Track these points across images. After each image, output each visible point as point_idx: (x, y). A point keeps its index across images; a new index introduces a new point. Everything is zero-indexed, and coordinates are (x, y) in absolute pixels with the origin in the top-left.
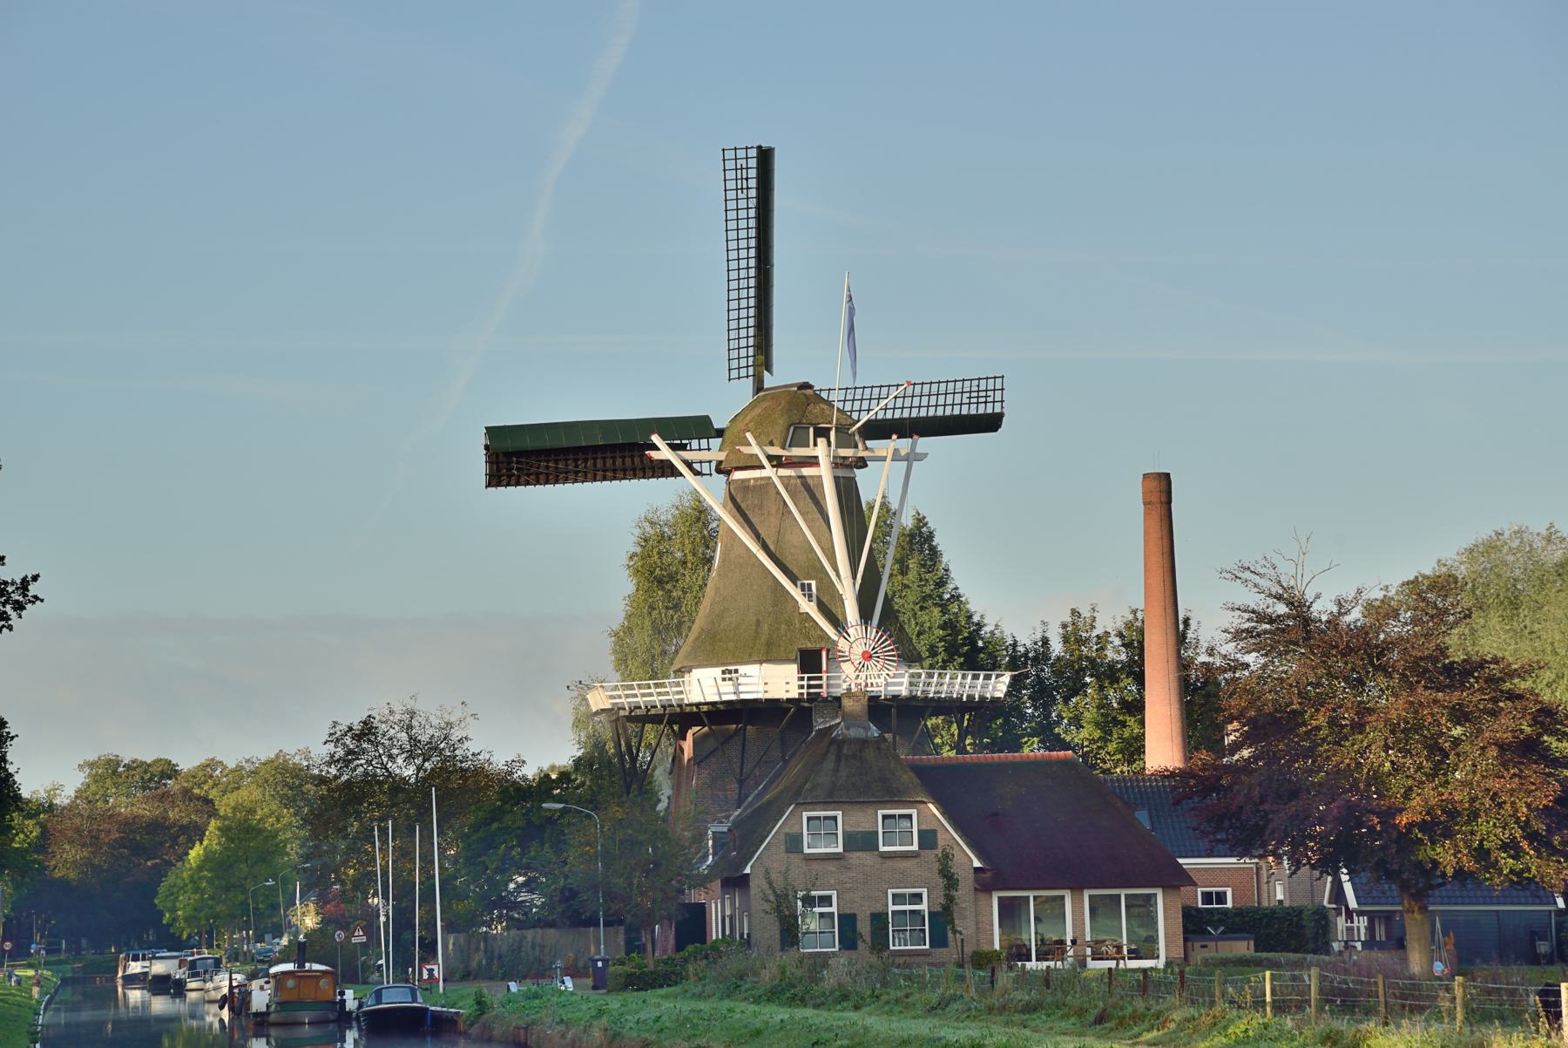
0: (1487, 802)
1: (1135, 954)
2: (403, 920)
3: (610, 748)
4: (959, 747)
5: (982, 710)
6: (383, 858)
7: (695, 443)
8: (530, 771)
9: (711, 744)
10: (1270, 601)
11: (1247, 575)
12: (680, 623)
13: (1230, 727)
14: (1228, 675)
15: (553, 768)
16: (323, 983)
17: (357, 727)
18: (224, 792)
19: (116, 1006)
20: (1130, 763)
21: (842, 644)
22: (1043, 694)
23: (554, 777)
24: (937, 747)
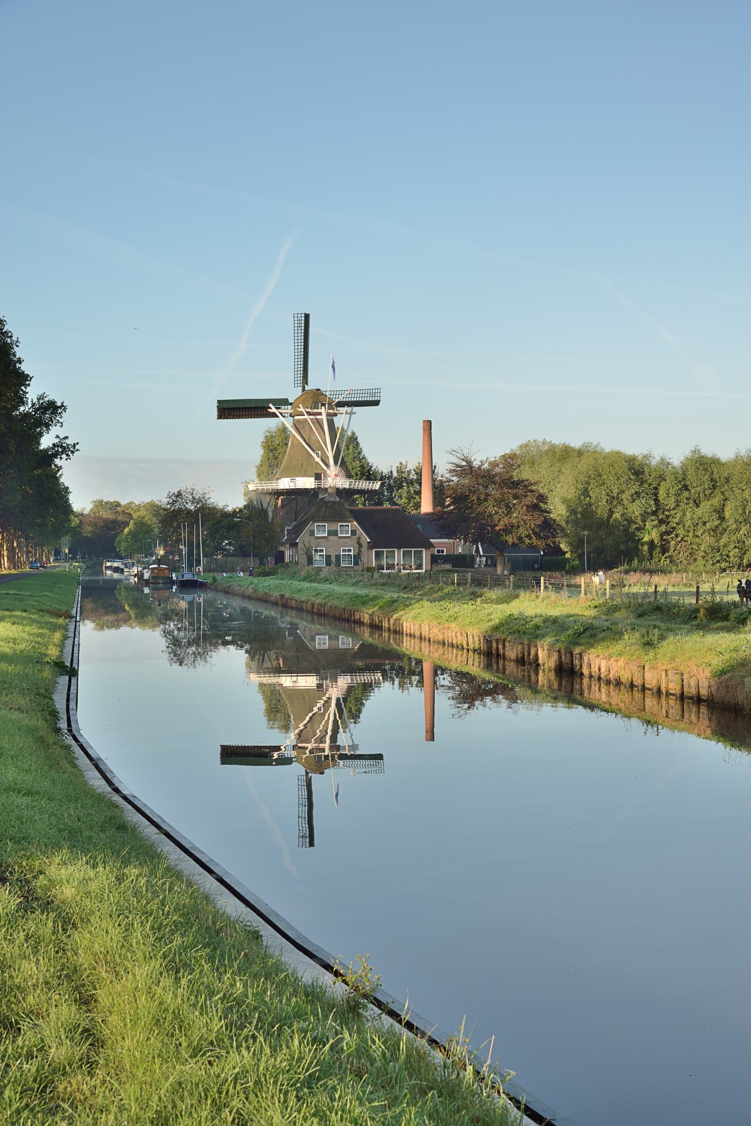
0: (523, 523)
1: (416, 569)
2: (190, 553)
3: (255, 502)
4: (364, 505)
5: (371, 493)
6: (184, 535)
7: (283, 407)
8: (230, 509)
9: (286, 502)
10: (461, 461)
11: (454, 453)
12: (278, 464)
13: (447, 500)
14: (447, 484)
15: (237, 508)
16: (166, 571)
17: (176, 493)
18: (135, 512)
19: (103, 575)
20: (416, 510)
21: (328, 472)
22: (390, 488)
23: (237, 510)
24: (357, 504)
